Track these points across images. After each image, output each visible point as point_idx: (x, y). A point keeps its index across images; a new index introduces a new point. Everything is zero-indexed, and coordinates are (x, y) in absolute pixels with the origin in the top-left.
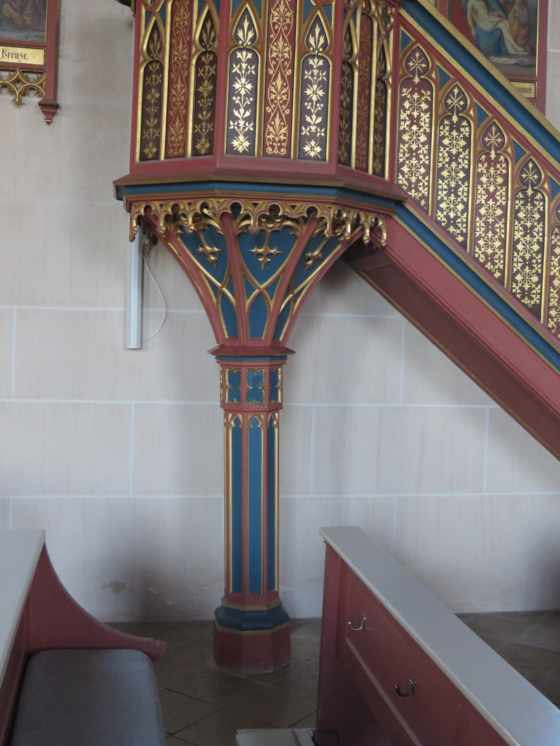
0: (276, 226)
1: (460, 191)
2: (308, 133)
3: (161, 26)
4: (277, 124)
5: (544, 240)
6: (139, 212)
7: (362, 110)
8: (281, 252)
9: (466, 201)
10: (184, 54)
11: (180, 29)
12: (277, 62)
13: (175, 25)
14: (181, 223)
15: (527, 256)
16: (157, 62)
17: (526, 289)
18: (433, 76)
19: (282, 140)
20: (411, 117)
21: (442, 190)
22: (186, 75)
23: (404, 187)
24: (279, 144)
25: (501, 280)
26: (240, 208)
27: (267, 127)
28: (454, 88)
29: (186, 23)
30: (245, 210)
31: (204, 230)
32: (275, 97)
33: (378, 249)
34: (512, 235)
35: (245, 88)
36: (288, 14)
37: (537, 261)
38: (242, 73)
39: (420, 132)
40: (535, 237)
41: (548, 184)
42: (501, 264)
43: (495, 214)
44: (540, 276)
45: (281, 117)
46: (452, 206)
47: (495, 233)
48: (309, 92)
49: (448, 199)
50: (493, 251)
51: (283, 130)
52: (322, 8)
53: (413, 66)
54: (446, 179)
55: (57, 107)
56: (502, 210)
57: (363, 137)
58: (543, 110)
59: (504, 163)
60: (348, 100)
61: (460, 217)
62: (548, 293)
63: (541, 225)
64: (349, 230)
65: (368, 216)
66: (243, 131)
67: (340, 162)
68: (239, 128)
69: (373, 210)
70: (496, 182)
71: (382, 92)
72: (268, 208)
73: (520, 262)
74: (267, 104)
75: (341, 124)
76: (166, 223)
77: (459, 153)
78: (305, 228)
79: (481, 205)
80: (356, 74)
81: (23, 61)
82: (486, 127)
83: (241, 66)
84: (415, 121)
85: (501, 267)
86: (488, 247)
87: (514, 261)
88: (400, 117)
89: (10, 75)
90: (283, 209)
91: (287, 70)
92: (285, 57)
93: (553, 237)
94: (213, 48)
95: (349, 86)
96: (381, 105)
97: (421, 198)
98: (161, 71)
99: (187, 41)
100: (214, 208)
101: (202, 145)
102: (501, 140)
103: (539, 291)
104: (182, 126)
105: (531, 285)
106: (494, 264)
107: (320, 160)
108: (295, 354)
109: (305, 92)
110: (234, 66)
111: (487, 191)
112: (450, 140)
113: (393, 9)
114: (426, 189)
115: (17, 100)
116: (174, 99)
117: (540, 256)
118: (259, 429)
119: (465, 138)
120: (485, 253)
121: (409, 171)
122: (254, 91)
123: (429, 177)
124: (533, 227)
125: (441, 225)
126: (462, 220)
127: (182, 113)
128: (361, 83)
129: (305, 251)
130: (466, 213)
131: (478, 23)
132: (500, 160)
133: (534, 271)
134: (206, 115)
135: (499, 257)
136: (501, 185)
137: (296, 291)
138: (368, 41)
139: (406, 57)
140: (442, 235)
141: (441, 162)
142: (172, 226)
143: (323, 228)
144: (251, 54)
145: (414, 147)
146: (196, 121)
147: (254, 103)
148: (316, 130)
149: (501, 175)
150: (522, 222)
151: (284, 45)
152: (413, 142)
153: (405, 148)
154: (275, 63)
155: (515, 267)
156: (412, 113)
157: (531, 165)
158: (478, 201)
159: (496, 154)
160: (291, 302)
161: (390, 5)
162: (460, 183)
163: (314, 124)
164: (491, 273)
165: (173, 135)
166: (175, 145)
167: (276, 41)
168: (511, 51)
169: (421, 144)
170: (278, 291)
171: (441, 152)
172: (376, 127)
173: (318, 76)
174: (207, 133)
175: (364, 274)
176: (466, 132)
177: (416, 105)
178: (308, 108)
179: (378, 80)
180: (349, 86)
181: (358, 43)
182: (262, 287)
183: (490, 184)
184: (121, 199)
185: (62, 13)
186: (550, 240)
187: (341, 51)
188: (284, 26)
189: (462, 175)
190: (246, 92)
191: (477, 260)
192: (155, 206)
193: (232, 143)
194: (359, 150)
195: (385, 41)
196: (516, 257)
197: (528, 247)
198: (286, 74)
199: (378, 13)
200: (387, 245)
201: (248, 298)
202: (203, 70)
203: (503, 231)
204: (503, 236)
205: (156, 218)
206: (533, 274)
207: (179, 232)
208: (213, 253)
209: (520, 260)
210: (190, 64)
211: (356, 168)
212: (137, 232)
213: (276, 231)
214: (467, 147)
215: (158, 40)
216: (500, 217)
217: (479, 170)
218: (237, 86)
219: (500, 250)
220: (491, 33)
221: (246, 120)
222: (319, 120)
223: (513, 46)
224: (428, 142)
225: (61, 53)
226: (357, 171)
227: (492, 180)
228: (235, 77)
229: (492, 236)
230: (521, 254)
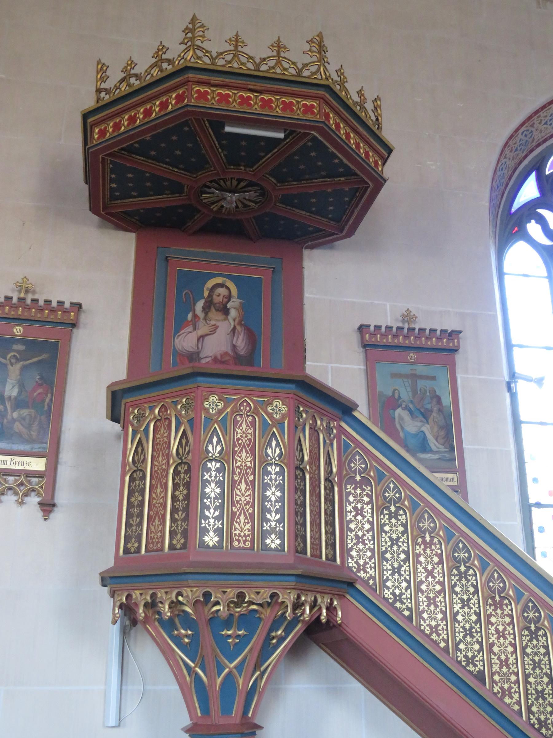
0: (243, 610)
1: (402, 571)
2: (268, 528)
3: (144, 442)
4: (242, 521)
5: (480, 610)
6: (121, 600)
7: (314, 506)
8: (248, 633)
9: (408, 579)
10: (163, 464)
11: (160, 444)
12: (241, 470)
13: (156, 441)
14: (158, 609)
15: (467, 626)
16: (141, 470)
17: (470, 656)
18: (372, 474)
19: (247, 535)
20: (355, 508)
21: (387, 570)
22: (164, 481)
23: (353, 569)
24: (244, 538)
25: (446, 650)
26: (211, 595)
27: (234, 524)
28: (390, 483)
29: (165, 439)
30: (216, 597)
31: (178, 615)
32: (240, 499)
33: (334, 626)
34: (452, 608)
35: (214, 492)
36: (249, 431)
37: (476, 630)
38: (212, 480)
39: (364, 520)
40: (472, 608)
41: (478, 560)
42: (445, 635)
43: (434, 589)
44: (481, 644)
45: (245, 515)
46: (397, 584)
47: (436, 606)
48: (268, 493)
49: (392, 578)
50: (436, 623)
51: (248, 526)
52: (277, 426)
53: (354, 467)
54: (390, 561)
55: (54, 505)
56: (441, 586)
57: (316, 528)
58: (466, 498)
59: (438, 544)
60: (302, 498)
61: (404, 594)
62: (489, 660)
63: (476, 597)
64: (308, 611)
65: (323, 597)
66: (213, 528)
67: (297, 551)
68: (209, 525)
69: (329, 591)
70: (433, 561)
71: (330, 490)
72: (235, 595)
73: (462, 632)
74: (233, 505)
75: (297, 519)
76: (145, 610)
77: (399, 538)
78: (269, 610)
79: (421, 582)
80: (308, 477)
81: (28, 468)
82: (419, 515)
83: (211, 474)
84: (359, 512)
85: (445, 637)
86: (432, 620)
87: (456, 631)
88: (346, 509)
89: (15, 479)
90: (249, 595)
91: (250, 476)
92: (248, 466)
93: (488, 607)
94: (188, 460)
95: (302, 487)
96: (330, 501)
97: (369, 578)
98: (144, 477)
99: (166, 454)
100: (188, 596)
101: (177, 540)
102: (433, 525)
103: (481, 658)
104: (161, 525)
105: (474, 653)
106: (439, 635)
107: (280, 551)
108: (264, 729)
109: (265, 493)
110: (205, 474)
111: (426, 569)
112: (390, 527)
113: (335, 423)
114: (373, 570)
115: (20, 500)
116: (155, 501)
117: (478, 626)
119: (402, 525)
120: (429, 625)
121: (357, 555)
122: (222, 494)
123: (375, 560)
124: (469, 600)
125: (389, 602)
126: (407, 596)
127: (161, 513)
128: (312, 484)
129: (271, 630)
130: (409, 590)
131: (405, 428)
132: (434, 542)
133: (475, 640)
134: (181, 515)
135: (443, 628)
136: (438, 564)
137: (262, 668)
138: (316, 449)
139: (348, 460)
140: (390, 611)
141: (384, 546)
142: (151, 612)
143: (286, 610)
144: (219, 464)
146: (173, 520)
147: (222, 506)
148: (276, 525)
149: (436, 555)
151: (246, 456)
152: (359, 530)
154: (239, 470)
155: (458, 637)
156: (356, 505)
157: (461, 545)
158: (419, 579)
159: (430, 537)
160: (258, 678)
161: (332, 420)
162: (402, 563)
163: (273, 520)
164: (436, 644)
165: (153, 531)
166: (154, 540)
167: (240, 453)
168: (434, 448)
169: (366, 531)
170: (246, 669)
171: (384, 537)
172: (327, 519)
173: (276, 480)
174: (182, 531)
175: (324, 647)
176: (403, 519)
177: (359, 498)
178: (268, 507)
179: (326, 480)
180: (302, 487)
181: (308, 452)
182: (232, 666)
183: (428, 563)
184: (106, 586)
185: (63, 429)
186: (485, 611)
187: (294, 460)
188: (246, 441)
189: (403, 556)
190: (215, 495)
191: (423, 632)
192: (136, 595)
193: (204, 539)
194: (313, 540)
195: (330, 449)
196: (457, 628)
197: (467, 617)
198: (248, 479)
199: (323, 426)
200: (342, 622)
201: (219, 677)
202: (179, 477)
203: (443, 604)
204: (444, 609)
205: (136, 605)
206: (474, 642)
207: (157, 617)
208: (187, 636)
209: (461, 630)
210: (168, 472)
211: (312, 555)
212: (118, 618)
213: (243, 614)
214: (405, 532)
215: (142, 453)
216: (439, 592)
217: (417, 552)
218: (207, 490)
219: (442, 622)
220: (415, 436)
221: (216, 518)
222: (278, 516)
223: (435, 445)
224: (372, 529)
225: (60, 460)
226: (313, 558)
227: (429, 559)
228: (206, 483)
229: (434, 609)
230: (462, 624)
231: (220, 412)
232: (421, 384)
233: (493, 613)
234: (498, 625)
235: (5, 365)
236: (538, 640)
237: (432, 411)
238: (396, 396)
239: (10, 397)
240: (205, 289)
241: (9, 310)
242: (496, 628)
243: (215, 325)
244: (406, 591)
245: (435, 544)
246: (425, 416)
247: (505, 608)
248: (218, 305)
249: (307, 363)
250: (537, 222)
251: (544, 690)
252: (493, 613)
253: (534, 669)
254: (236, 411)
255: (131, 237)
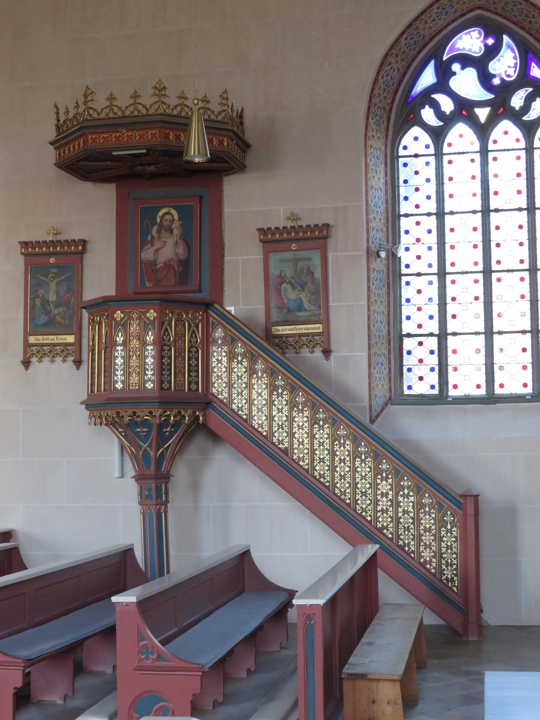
15: (280, 423)
20: (217, 360)
21: (234, 394)
36: (137, 328)
45: (136, 373)
46: (240, 401)
47: (262, 413)
64: (172, 418)
77: (242, 375)
84: (219, 361)
88: (212, 360)
89: (320, 338)
97: (224, 399)
103: (287, 441)
106: (263, 428)
111: (257, 392)
117: (287, 423)
118: (152, 513)
120: (258, 423)
124: (282, 408)
133: (284, 431)
145: (220, 374)
150: (277, 406)
153: (215, 375)
159: (261, 374)
162: (243, 389)
168: (307, 308)
173: (151, 353)
203: (266, 411)
209: (277, 425)
218: (117, 361)
220: (296, 300)
227: (260, 386)
230: (277, 422)
231: (122, 319)
232: (300, 264)
233: (297, 416)
234: (299, 422)
235: (48, 283)
236: (323, 430)
237: (307, 283)
238: (283, 275)
239: (52, 301)
240: (158, 217)
241: (263, 237)
242: (298, 424)
243: (164, 241)
244: (245, 405)
245: (264, 378)
246: (303, 287)
247: (304, 412)
248: (166, 227)
249: (226, 258)
250: (430, 107)
251: (324, 458)
252: (297, 416)
253: (319, 446)
254: (130, 318)
255: (114, 185)
